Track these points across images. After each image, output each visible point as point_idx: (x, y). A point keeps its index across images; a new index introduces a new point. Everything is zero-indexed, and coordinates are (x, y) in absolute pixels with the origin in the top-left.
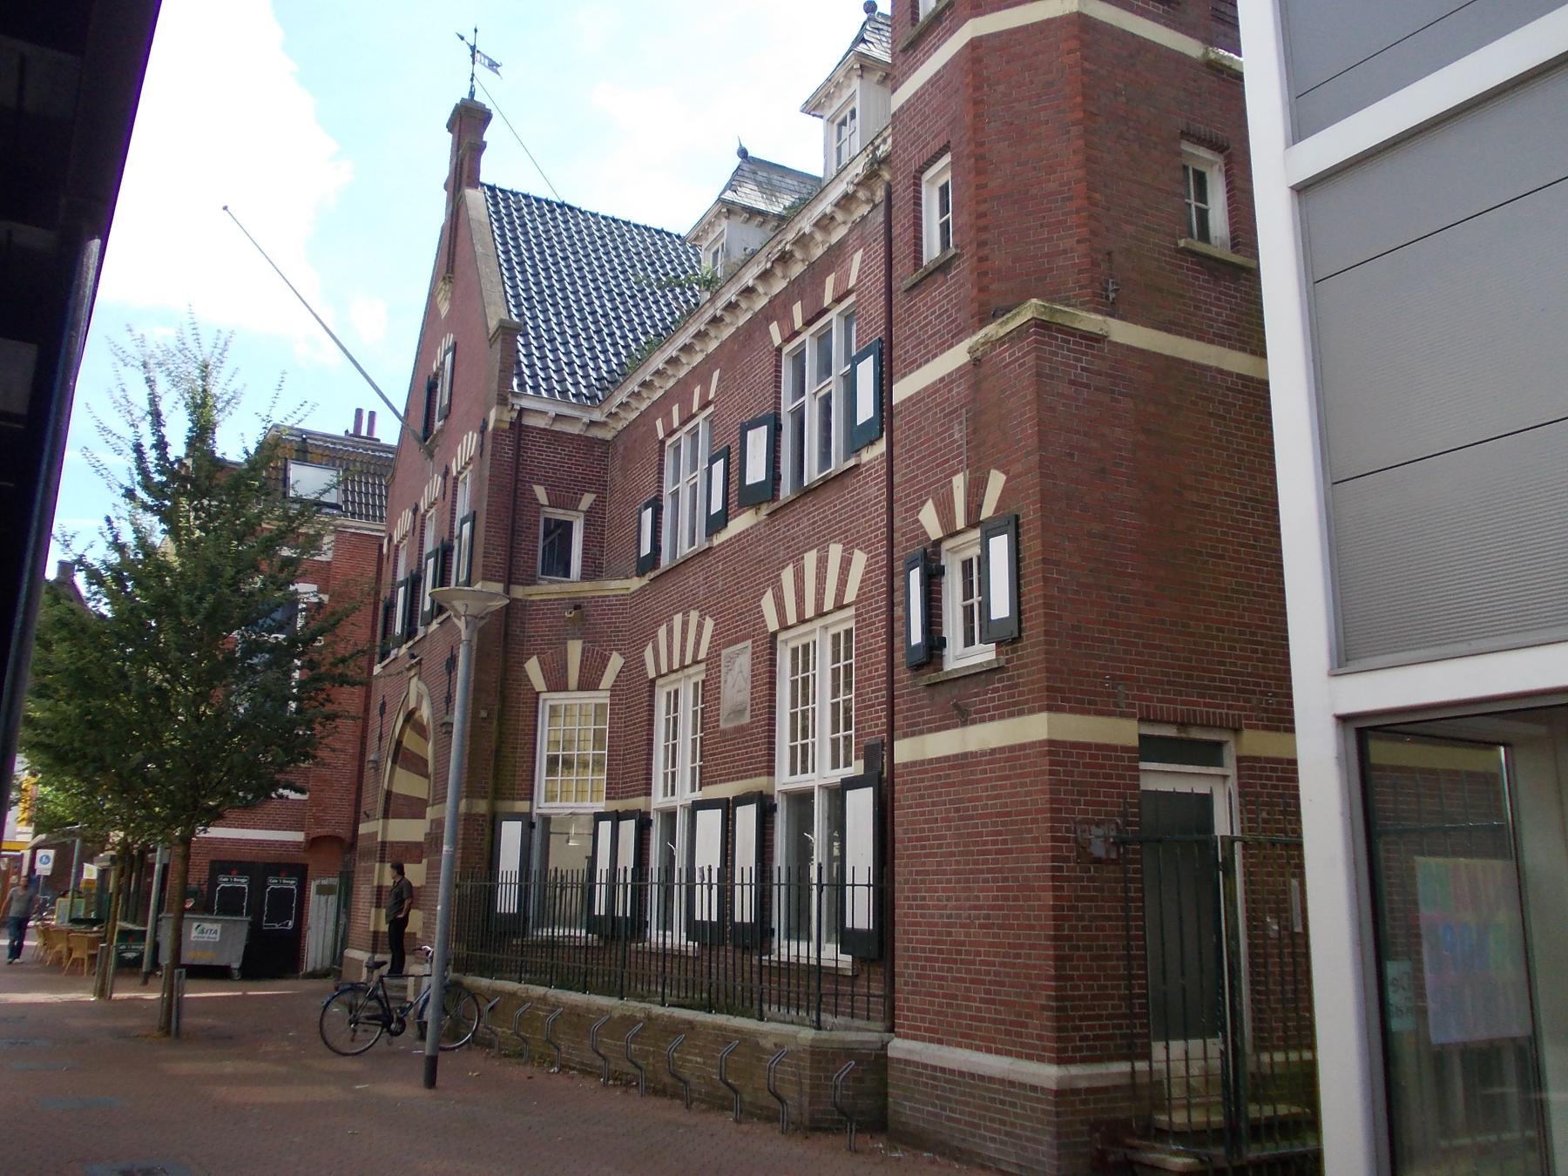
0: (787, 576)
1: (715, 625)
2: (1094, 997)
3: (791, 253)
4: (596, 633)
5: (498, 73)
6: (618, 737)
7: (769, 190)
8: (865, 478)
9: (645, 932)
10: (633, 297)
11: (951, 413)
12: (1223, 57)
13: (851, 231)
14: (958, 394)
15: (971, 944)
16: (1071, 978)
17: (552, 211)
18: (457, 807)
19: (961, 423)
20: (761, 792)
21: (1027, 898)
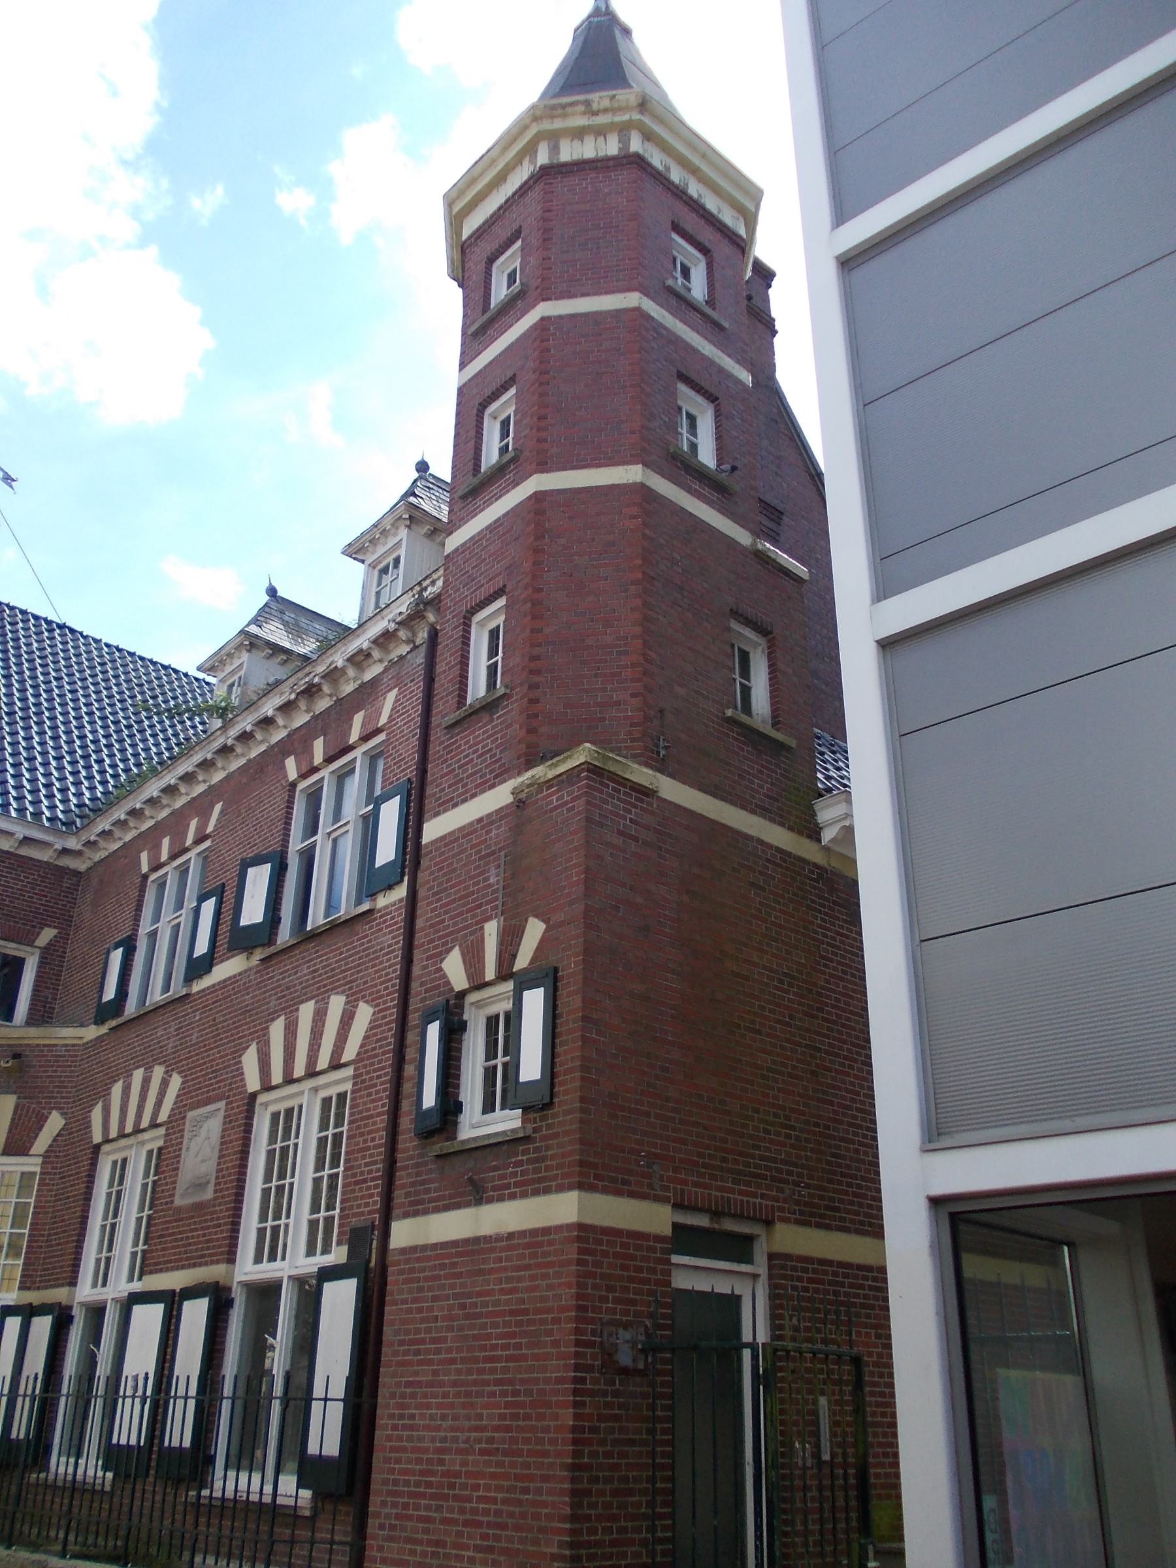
0: (277, 1030)
1: (183, 1083)
2: (613, 1543)
3: (318, 687)
4: (35, 1087)
5: (11, 487)
7: (295, 630)
8: (378, 925)
10: (129, 727)
11: (489, 855)
12: (769, 549)
13: (386, 670)
14: (497, 835)
15: (469, 1475)
16: (588, 1518)
17: (51, 631)
19: (499, 866)
20: (217, 1283)
21: (541, 1417)
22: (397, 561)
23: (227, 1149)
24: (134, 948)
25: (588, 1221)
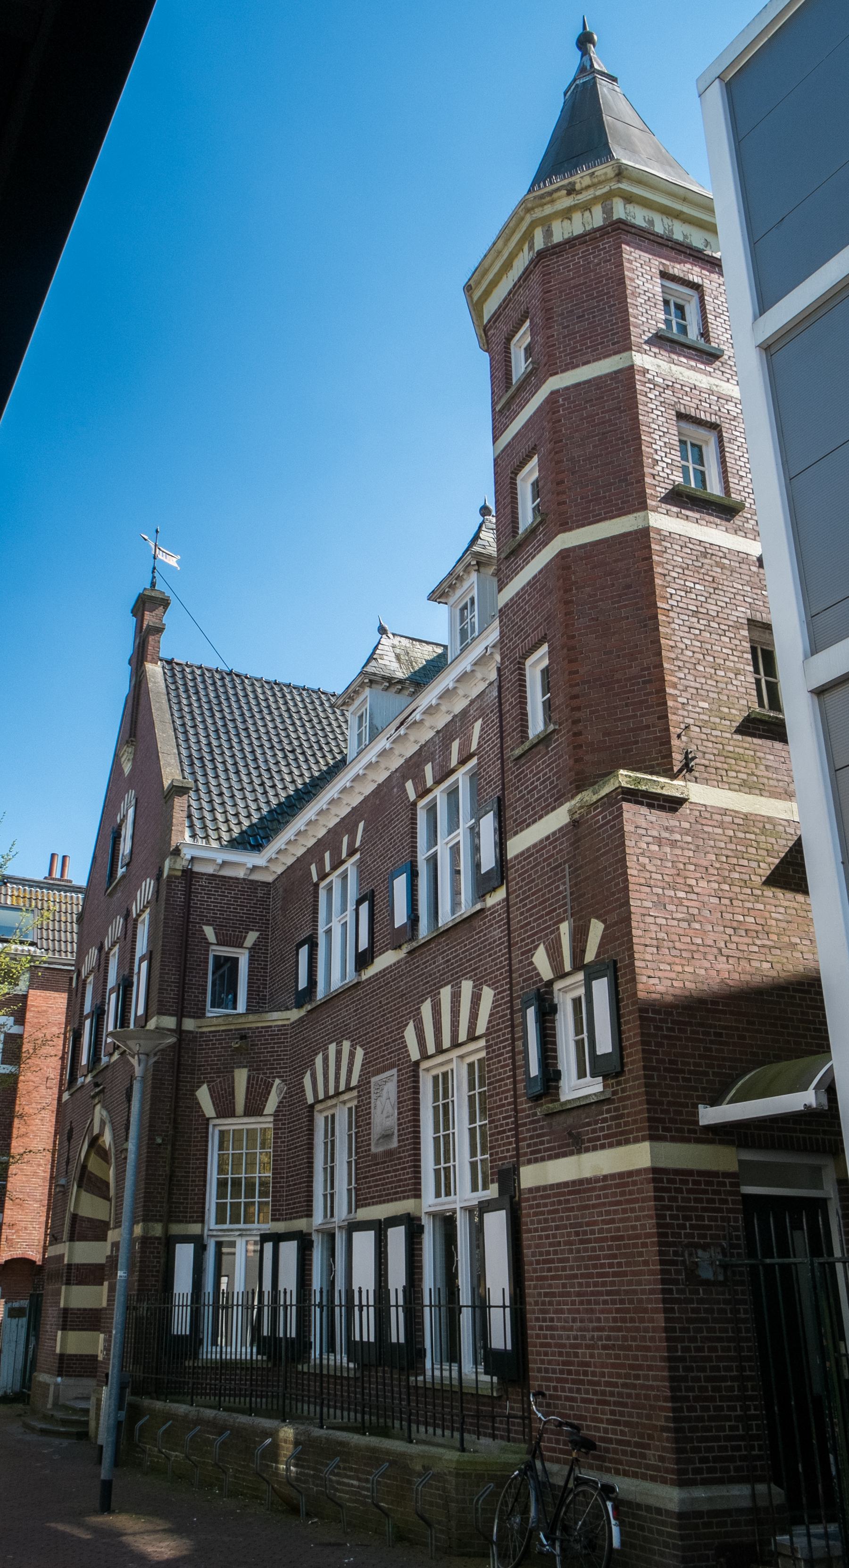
0: (426, 1009)
1: (365, 1054)
2: (711, 1419)
4: (261, 1061)
6: (281, 1160)
9: (310, 1353)
16: (686, 1399)
17: (223, 679)
18: (131, 1232)
21: (642, 1320)
22: (472, 600)
23: (403, 1107)
24: (317, 945)
25: (661, 1165)
